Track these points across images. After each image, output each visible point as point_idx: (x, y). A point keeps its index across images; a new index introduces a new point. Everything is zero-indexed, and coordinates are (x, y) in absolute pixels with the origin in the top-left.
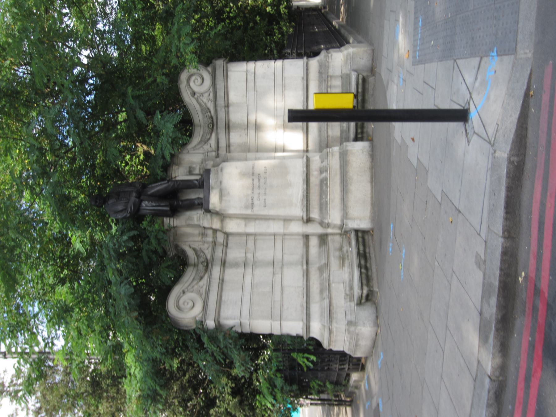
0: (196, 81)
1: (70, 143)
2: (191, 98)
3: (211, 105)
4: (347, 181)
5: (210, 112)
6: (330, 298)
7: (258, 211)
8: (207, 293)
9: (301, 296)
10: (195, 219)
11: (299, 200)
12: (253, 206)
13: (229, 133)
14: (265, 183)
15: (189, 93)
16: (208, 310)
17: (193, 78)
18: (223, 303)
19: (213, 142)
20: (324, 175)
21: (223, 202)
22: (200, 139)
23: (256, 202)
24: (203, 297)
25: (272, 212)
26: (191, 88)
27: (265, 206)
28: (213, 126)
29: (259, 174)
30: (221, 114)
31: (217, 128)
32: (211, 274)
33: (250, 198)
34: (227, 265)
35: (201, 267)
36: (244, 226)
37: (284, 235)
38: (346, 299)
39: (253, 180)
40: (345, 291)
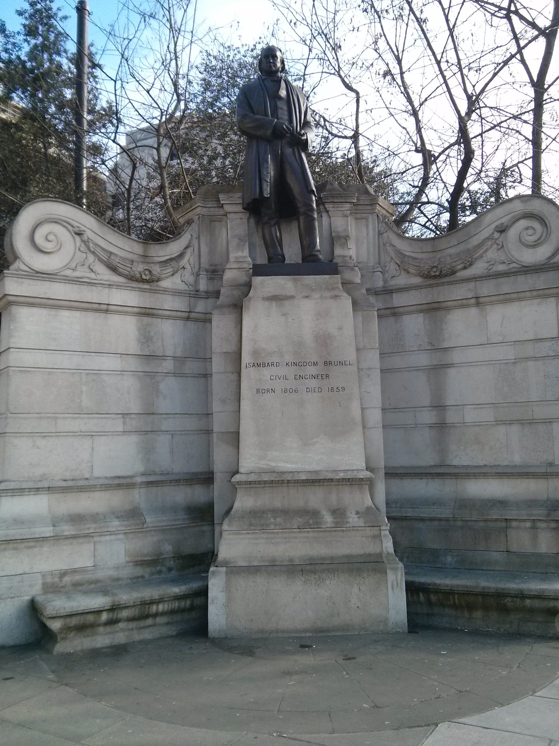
0: (530, 232)
1: (479, 208)
2: (493, 226)
3: (479, 268)
4: (314, 572)
5: (465, 268)
6: (57, 538)
7: (249, 377)
8: (77, 281)
9: (68, 475)
10: (240, 254)
11: (273, 464)
12: (259, 365)
13: (421, 311)
14: (308, 390)
15: (504, 220)
16: (31, 282)
17: (537, 225)
18: (53, 312)
19: (402, 280)
20: (328, 519)
21: (267, 303)
22: (407, 254)
23: (267, 372)
24: (68, 273)
25: (245, 406)
26: (514, 222)
27: (258, 391)
28: (435, 277)
29: (327, 376)
30: (461, 292)
31: (431, 286)
32: (119, 286)
33: (275, 359)
34: (146, 319)
35: (139, 268)
36: (225, 351)
37: (209, 432)
38: (52, 573)
39: (315, 364)
40: (74, 571)
